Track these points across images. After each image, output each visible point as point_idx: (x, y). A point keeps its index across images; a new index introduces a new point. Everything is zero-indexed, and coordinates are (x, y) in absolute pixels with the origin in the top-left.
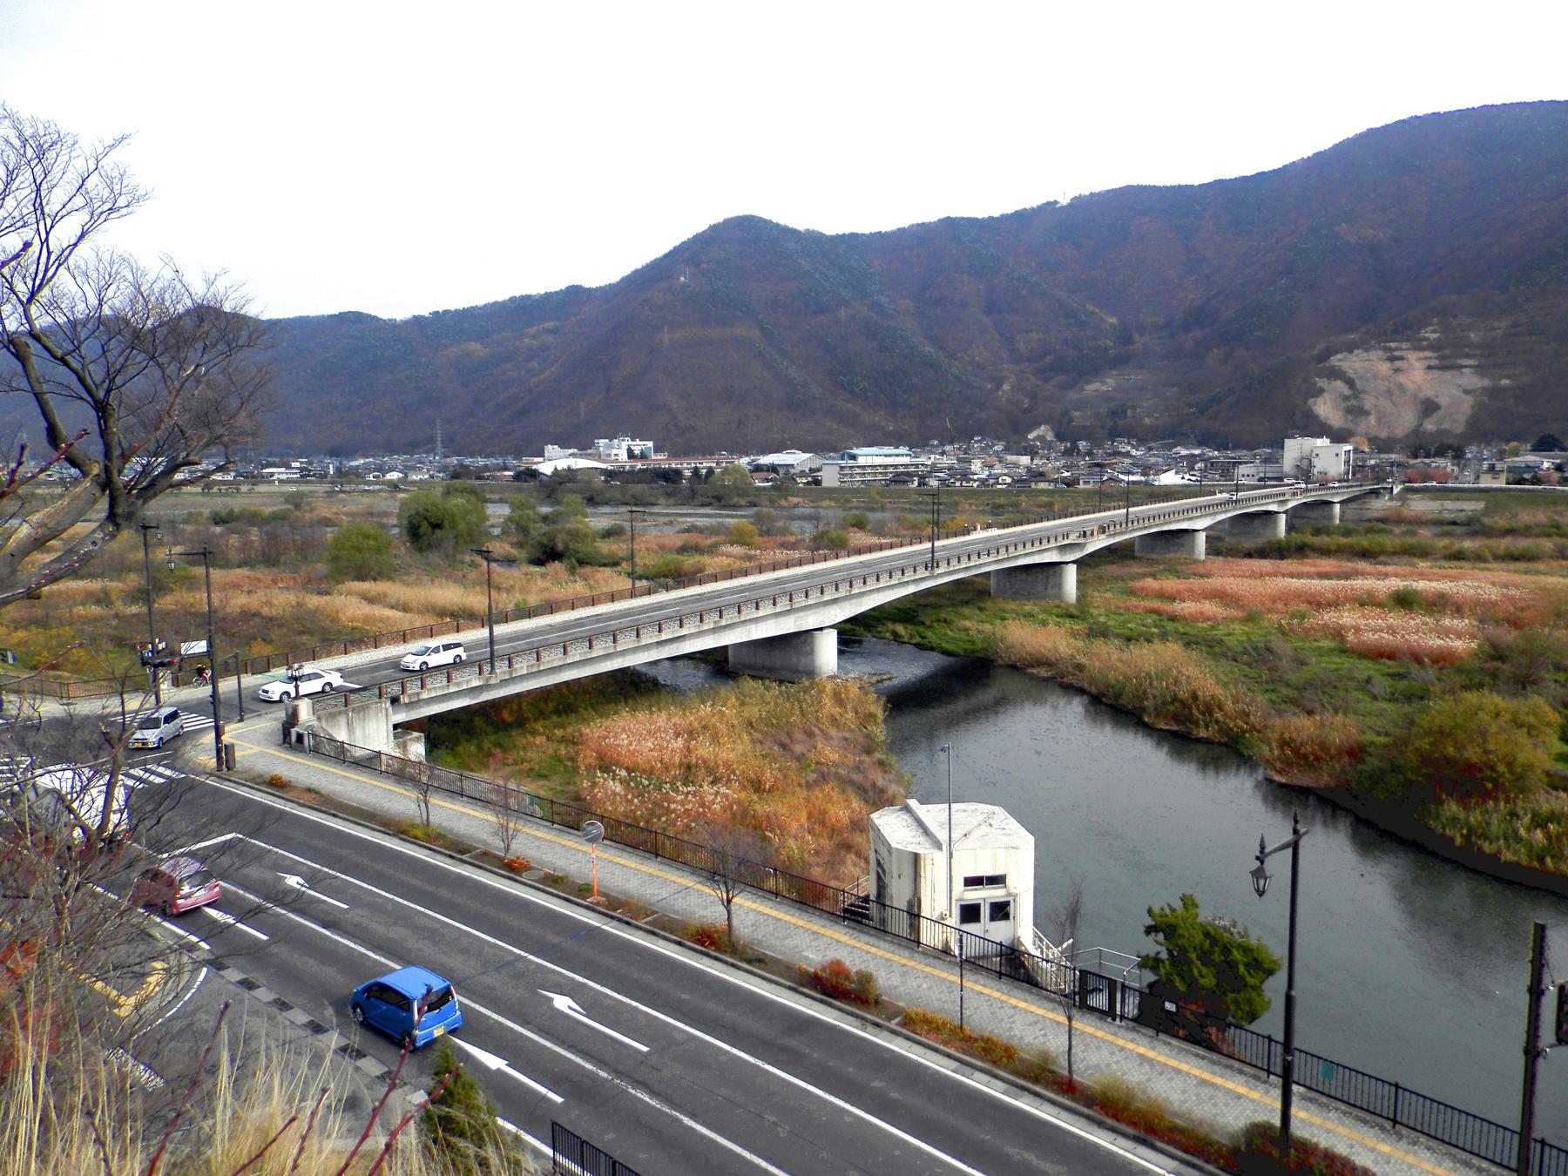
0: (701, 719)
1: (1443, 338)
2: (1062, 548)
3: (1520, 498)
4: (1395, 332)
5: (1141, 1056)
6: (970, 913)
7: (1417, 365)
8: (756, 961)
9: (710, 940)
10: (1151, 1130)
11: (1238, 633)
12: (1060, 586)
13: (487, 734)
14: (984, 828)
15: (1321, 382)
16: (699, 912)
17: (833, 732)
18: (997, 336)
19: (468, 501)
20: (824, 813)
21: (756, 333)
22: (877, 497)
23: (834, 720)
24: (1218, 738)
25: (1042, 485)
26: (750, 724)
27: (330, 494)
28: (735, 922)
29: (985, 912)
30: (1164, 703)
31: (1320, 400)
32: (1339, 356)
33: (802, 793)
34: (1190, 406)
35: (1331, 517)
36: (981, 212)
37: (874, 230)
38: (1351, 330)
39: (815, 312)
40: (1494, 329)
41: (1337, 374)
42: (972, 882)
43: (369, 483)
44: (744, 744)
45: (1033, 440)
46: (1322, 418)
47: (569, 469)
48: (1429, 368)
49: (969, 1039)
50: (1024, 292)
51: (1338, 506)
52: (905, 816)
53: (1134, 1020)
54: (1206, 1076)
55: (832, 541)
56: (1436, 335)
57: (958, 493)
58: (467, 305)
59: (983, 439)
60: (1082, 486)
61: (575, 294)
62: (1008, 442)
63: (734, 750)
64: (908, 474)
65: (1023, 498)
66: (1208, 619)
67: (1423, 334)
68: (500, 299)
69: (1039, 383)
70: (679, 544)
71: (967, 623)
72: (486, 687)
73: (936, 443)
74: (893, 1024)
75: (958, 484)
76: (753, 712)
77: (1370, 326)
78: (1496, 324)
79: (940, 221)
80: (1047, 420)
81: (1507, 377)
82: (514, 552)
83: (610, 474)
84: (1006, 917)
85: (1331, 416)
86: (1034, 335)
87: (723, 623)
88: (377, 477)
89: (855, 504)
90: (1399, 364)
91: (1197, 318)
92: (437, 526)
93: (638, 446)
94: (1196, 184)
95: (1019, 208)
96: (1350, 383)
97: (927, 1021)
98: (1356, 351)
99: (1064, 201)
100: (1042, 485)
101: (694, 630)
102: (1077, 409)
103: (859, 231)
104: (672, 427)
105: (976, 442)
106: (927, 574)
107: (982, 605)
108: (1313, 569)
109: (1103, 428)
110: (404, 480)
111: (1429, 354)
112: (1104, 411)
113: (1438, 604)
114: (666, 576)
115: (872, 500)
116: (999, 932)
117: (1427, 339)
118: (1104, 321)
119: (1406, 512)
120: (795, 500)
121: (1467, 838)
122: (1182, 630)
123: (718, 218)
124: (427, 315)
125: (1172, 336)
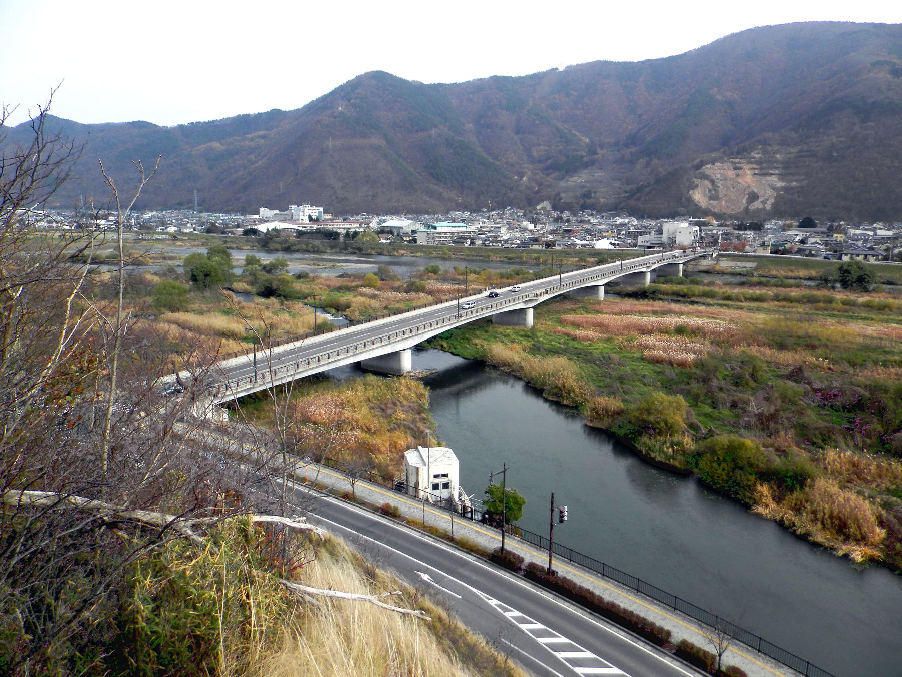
0: (347, 398)
1: (763, 157)
2: (526, 302)
3: (777, 262)
4: (738, 153)
5: (477, 531)
6: (436, 487)
7: (748, 172)
8: (363, 504)
9: (348, 497)
10: (472, 550)
11: (599, 348)
12: (525, 320)
13: (250, 403)
14: (443, 457)
15: (697, 181)
16: (343, 487)
17: (405, 403)
18: (522, 148)
19: (222, 258)
20: (395, 443)
21: (382, 142)
22: (447, 251)
23: (405, 396)
24: (572, 404)
25: (535, 247)
26: (369, 400)
27: (137, 241)
28: (355, 491)
29: (441, 486)
30: (552, 388)
31: (696, 191)
32: (708, 166)
33: (388, 434)
34: (626, 192)
35: (678, 271)
36: (514, 74)
37: (452, 82)
38: (716, 150)
39: (417, 131)
40: (790, 153)
41: (705, 177)
42: (436, 476)
43: (159, 233)
44: (365, 410)
45: (540, 210)
46: (696, 201)
47: (275, 230)
48: (755, 174)
49: (425, 527)
50: (537, 122)
51: (681, 265)
52: (416, 453)
53: (480, 521)
54: (494, 536)
55: (417, 287)
56: (759, 156)
57: (491, 250)
58: (211, 119)
59: (512, 208)
60: (557, 248)
61: (275, 115)
62: (525, 210)
63: (362, 414)
64: (465, 238)
65: (525, 254)
66: (590, 340)
67: (752, 155)
68: (231, 116)
69: (543, 175)
70: (338, 285)
71: (477, 341)
72: (253, 388)
73: (485, 210)
74: (403, 523)
75: (491, 244)
76: (371, 393)
77: (726, 148)
78: (792, 151)
79: (491, 77)
80: (548, 198)
81: (796, 181)
82: (249, 288)
83: (300, 233)
84: (448, 488)
85: (701, 201)
86: (542, 148)
87: (357, 352)
88: (163, 229)
89: (435, 255)
90: (739, 171)
91: (633, 140)
92: (207, 275)
93: (315, 211)
94: (636, 61)
95: (536, 71)
96: (712, 182)
97: (414, 522)
98: (716, 164)
99: (562, 68)
100: (535, 247)
101: (344, 356)
102: (564, 192)
103: (444, 82)
104: (334, 197)
105: (508, 210)
106: (455, 321)
107: (486, 329)
108: (650, 309)
109: (578, 203)
110: (180, 232)
111: (755, 166)
112: (578, 194)
113: (695, 332)
114: (331, 307)
115: (444, 253)
116: (443, 494)
117: (754, 158)
118: (582, 140)
119: (717, 268)
120: (402, 252)
121: (647, 451)
122: (576, 346)
123: (361, 71)
124: (186, 124)
125: (619, 151)
